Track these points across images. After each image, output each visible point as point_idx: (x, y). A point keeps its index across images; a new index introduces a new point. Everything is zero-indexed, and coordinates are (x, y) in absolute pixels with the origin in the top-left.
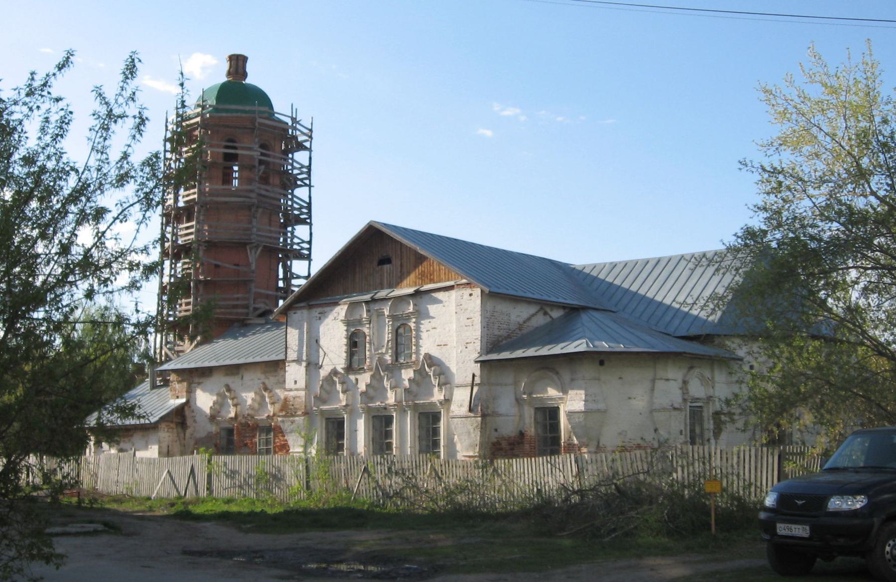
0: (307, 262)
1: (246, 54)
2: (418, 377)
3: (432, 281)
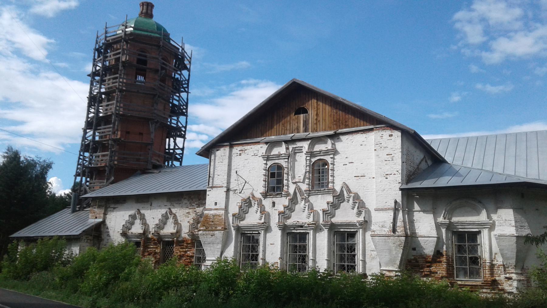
0: (183, 139)
1: (153, 4)
2: (336, 201)
3: (347, 126)
